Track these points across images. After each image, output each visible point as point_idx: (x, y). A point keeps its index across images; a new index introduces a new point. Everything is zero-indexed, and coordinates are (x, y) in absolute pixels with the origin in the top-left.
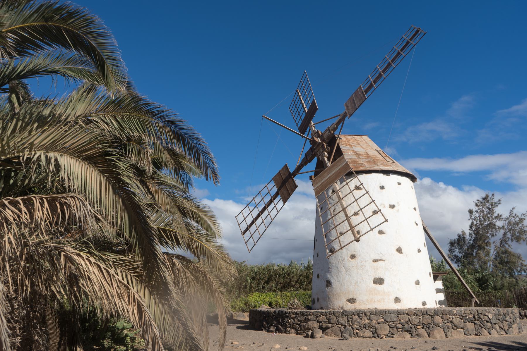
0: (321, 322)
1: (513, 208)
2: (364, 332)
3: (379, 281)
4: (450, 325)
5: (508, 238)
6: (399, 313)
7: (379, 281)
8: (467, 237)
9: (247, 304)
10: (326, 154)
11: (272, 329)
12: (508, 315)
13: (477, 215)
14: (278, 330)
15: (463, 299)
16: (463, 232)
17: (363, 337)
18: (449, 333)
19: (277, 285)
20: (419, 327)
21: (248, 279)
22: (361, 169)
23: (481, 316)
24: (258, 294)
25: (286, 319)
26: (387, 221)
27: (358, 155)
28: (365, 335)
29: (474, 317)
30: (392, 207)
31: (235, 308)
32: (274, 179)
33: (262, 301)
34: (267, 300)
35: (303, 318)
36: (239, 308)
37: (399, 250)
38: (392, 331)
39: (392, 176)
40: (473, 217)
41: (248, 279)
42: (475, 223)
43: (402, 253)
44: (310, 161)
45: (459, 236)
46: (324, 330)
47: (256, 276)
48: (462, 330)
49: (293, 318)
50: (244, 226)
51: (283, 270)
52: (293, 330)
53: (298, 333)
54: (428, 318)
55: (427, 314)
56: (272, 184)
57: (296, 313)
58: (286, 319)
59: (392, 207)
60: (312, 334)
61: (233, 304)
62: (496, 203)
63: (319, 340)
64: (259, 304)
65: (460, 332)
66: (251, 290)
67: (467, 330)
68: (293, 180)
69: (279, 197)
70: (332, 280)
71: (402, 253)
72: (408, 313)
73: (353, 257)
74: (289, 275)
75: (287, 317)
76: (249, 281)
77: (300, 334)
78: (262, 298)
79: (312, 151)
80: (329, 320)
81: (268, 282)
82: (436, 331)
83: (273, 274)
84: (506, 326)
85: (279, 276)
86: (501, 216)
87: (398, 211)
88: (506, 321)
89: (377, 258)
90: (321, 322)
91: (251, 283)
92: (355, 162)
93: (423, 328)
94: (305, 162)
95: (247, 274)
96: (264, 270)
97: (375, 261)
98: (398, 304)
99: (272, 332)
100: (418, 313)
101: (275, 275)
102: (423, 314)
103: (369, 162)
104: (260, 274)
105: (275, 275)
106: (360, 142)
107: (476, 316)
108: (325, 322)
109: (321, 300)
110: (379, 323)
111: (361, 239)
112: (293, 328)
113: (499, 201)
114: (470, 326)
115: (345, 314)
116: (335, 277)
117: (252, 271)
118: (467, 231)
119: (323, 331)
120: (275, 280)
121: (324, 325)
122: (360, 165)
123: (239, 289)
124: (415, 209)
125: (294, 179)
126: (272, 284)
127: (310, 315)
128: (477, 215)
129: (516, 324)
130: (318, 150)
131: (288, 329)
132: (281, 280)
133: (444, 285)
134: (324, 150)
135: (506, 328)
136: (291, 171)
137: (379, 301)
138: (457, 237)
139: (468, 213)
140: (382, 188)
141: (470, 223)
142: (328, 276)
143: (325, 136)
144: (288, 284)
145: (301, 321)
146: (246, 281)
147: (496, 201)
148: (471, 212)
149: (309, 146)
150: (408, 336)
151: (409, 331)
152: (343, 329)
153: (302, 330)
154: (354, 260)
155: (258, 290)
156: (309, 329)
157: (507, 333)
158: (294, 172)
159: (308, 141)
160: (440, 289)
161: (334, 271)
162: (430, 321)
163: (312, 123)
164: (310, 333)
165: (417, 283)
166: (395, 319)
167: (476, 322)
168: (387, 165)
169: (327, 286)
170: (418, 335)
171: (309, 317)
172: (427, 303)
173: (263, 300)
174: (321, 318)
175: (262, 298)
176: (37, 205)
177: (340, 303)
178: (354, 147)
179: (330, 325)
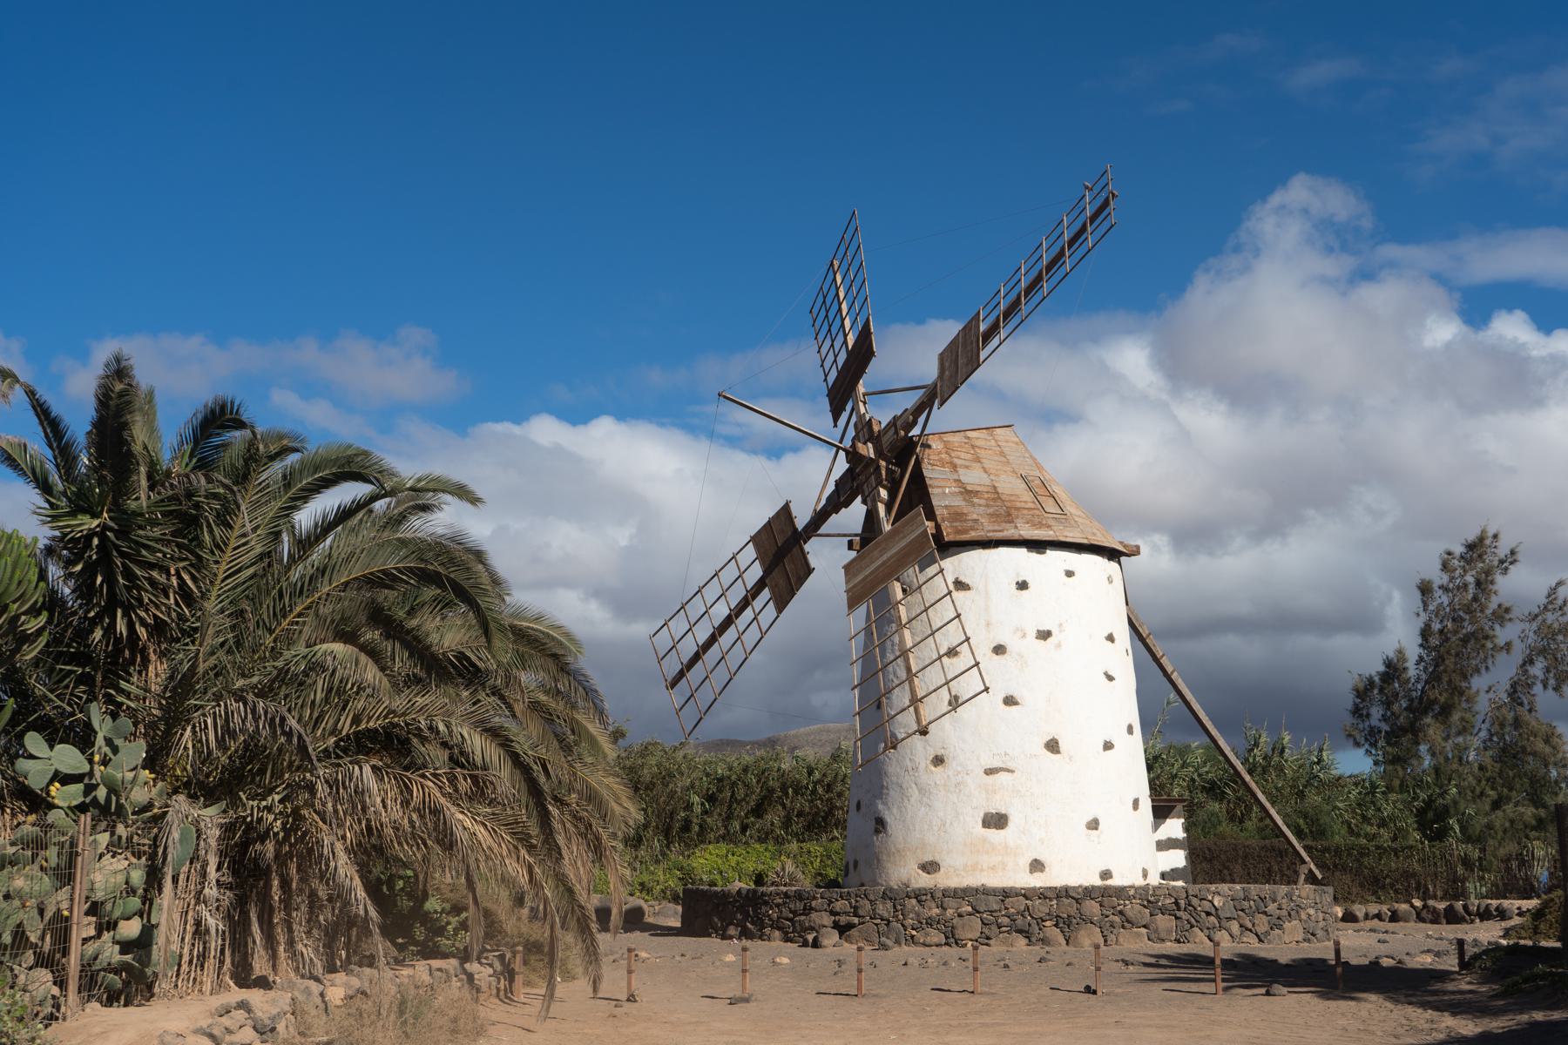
0: (837, 914)
1: (1559, 584)
2: (927, 935)
3: (996, 821)
4: (1117, 919)
5: (1535, 677)
6: (1043, 894)
7: (996, 821)
8: (1412, 672)
9: (687, 876)
10: (884, 493)
11: (732, 931)
12: (1274, 901)
13: (1445, 600)
14: (745, 934)
15: (1335, 866)
16: (1400, 652)
17: (924, 945)
18: (1111, 938)
19: (787, 824)
20: (1048, 923)
21: (696, 799)
22: (973, 535)
23: (1195, 901)
24: (723, 848)
25: (764, 909)
26: (987, 689)
27: (968, 493)
28: (928, 940)
29: (1176, 903)
30: (1044, 635)
31: (649, 891)
32: (755, 539)
33: (721, 865)
34: (750, 866)
35: (799, 906)
36: (663, 891)
37: (1053, 746)
38: (986, 930)
39: (1051, 554)
40: (1431, 608)
41: (696, 799)
42: (1436, 626)
43: (1058, 752)
44: (847, 504)
45: (1389, 664)
46: (843, 930)
47: (720, 791)
48: (1144, 930)
49: (778, 905)
50: (672, 666)
51: (810, 772)
52: (777, 933)
53: (787, 940)
54: (1070, 905)
55: (1068, 896)
56: (751, 552)
57: (786, 895)
58: (764, 909)
59: (1044, 635)
60: (815, 939)
61: (645, 878)
62: (1502, 562)
63: (830, 950)
64: (723, 878)
65: (1139, 935)
66: (702, 837)
67: (1156, 931)
68: (802, 550)
69: (766, 594)
70: (889, 819)
71: (1058, 752)
72: (1064, 893)
73: (938, 761)
74: (829, 788)
75: (766, 903)
76: (698, 809)
77: (791, 941)
78: (733, 860)
79: (853, 480)
80: (856, 908)
81: (758, 811)
82: (1082, 932)
83: (776, 785)
84: (1262, 924)
85: (796, 792)
86: (1507, 610)
87: (1059, 646)
88: (1265, 913)
89: (996, 764)
90: (837, 914)
91: (705, 812)
92: (957, 516)
93: (1056, 925)
94: (837, 501)
95: (692, 786)
96: (745, 770)
97: (990, 772)
98: (1037, 875)
99: (731, 938)
100: (1049, 894)
101: (784, 789)
102: (1058, 897)
103: (994, 516)
104: (734, 784)
105: (784, 789)
106: (982, 453)
107: (1182, 903)
108: (847, 913)
109: (861, 866)
110: (960, 916)
111: (932, 728)
112: (779, 929)
113: (1513, 553)
114: (1164, 922)
115: (920, 895)
116: (895, 811)
117: (708, 775)
118: (1413, 651)
119: (841, 934)
120: (784, 806)
121: (843, 920)
122: (970, 524)
123: (667, 833)
124: (1110, 638)
125: (807, 547)
126: (774, 817)
127: (815, 898)
128: (1445, 600)
129: (1294, 922)
130: (867, 479)
131: (768, 931)
132: (801, 803)
133: (1187, 829)
134: (880, 483)
135: (1261, 929)
136: (800, 523)
137: (993, 868)
138: (1382, 668)
139: (1418, 594)
140: (1022, 586)
141: (1419, 623)
142: (880, 807)
143: (886, 440)
144: (825, 819)
145: (794, 912)
146: (689, 807)
147: (1502, 556)
148: (1425, 589)
149: (842, 465)
150: (1021, 941)
151: (1025, 933)
152: (883, 928)
153: (799, 933)
154: (940, 769)
155: (726, 837)
156: (812, 929)
157: (1261, 941)
158: (806, 527)
159: (842, 454)
160: (1177, 840)
161: (893, 794)
162: (1073, 911)
163: (861, 389)
164: (810, 938)
165: (1094, 825)
166: (995, 907)
167: (1179, 914)
168: (1040, 525)
169: (877, 832)
170: (1044, 941)
171: (814, 903)
172: (1114, 874)
173: (737, 868)
174: (840, 905)
175: (733, 860)
176: (461, 778)
177: (904, 872)
178: (961, 471)
179: (856, 920)
